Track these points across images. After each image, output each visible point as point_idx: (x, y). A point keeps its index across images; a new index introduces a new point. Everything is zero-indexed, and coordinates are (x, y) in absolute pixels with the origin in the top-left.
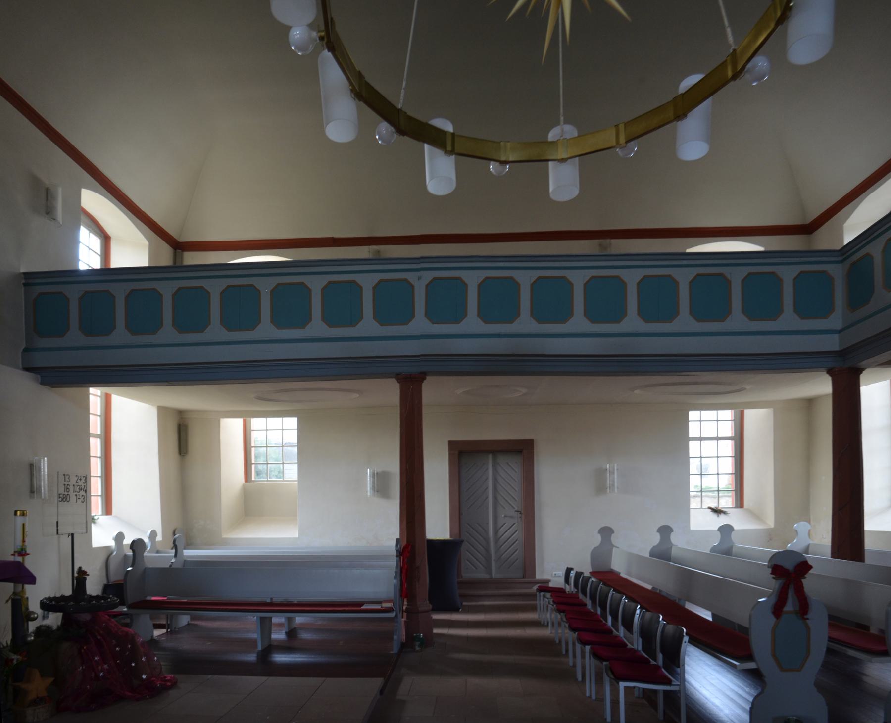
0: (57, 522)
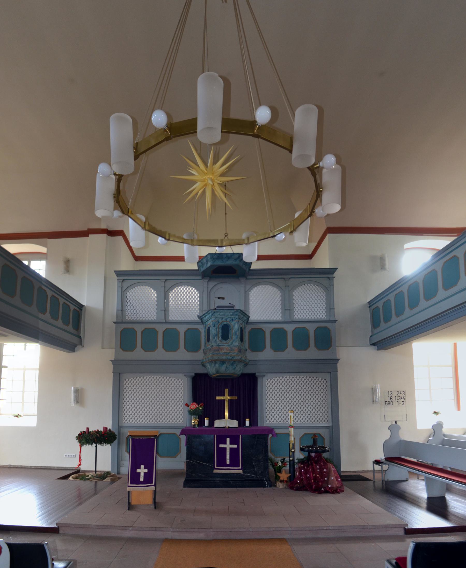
0: (407, 415)
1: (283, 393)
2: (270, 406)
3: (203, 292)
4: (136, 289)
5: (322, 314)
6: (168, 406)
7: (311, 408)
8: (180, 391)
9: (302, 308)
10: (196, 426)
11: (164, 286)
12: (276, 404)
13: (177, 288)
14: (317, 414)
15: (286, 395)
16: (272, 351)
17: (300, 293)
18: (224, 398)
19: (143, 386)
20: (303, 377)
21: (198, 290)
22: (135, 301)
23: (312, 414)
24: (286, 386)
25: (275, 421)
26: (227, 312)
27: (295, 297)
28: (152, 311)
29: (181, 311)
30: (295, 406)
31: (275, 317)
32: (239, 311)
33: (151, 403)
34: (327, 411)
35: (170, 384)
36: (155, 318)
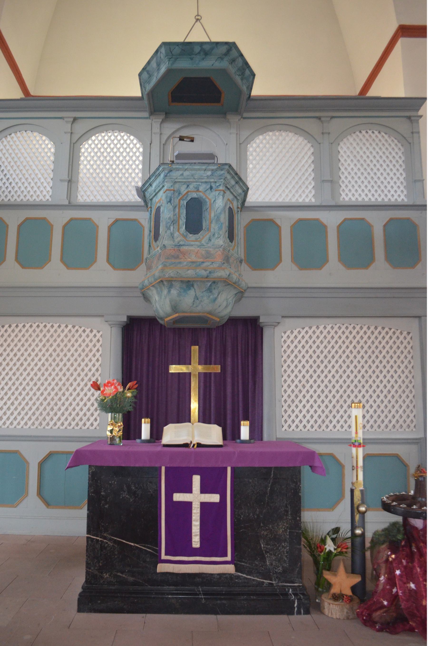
1: (318, 362)
2: (289, 391)
3: (151, 144)
4: (12, 138)
5: (399, 192)
6: (68, 390)
7: (378, 396)
8: (94, 355)
9: (356, 178)
10: (118, 440)
11: (70, 131)
12: (304, 386)
13: (97, 135)
14: (393, 411)
15: (326, 367)
16: (295, 268)
17: (351, 148)
18: (188, 368)
19: (16, 345)
20: (361, 328)
21: (140, 140)
22: (10, 162)
23: (383, 412)
24: (325, 347)
25: (301, 427)
26: (199, 170)
27: (342, 156)
28: (39, 179)
29: (104, 183)
30: (345, 391)
31: (300, 196)
32: (227, 167)
33: (31, 384)
34: (414, 403)
35: (73, 340)
36: (48, 197)
